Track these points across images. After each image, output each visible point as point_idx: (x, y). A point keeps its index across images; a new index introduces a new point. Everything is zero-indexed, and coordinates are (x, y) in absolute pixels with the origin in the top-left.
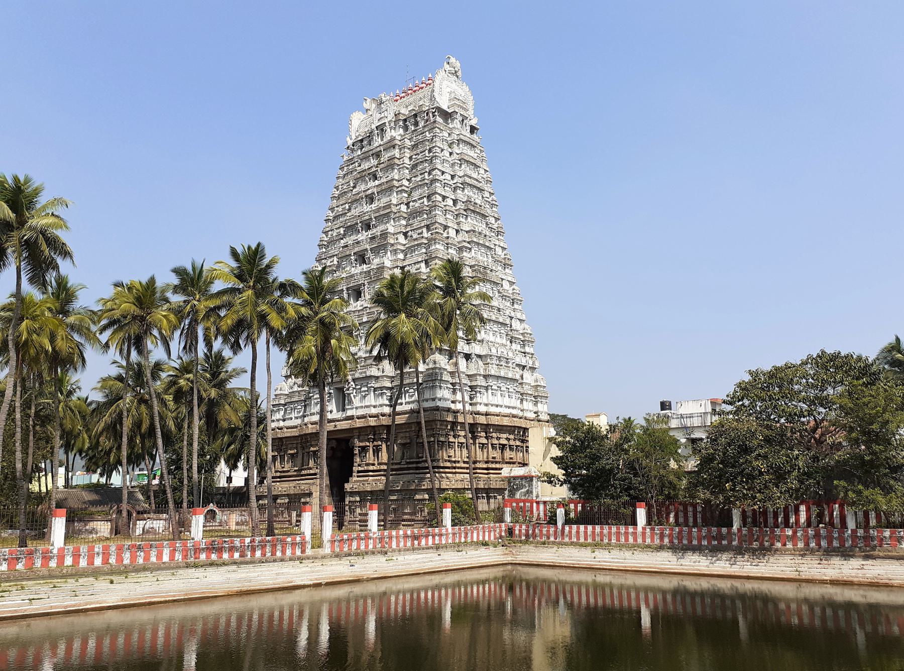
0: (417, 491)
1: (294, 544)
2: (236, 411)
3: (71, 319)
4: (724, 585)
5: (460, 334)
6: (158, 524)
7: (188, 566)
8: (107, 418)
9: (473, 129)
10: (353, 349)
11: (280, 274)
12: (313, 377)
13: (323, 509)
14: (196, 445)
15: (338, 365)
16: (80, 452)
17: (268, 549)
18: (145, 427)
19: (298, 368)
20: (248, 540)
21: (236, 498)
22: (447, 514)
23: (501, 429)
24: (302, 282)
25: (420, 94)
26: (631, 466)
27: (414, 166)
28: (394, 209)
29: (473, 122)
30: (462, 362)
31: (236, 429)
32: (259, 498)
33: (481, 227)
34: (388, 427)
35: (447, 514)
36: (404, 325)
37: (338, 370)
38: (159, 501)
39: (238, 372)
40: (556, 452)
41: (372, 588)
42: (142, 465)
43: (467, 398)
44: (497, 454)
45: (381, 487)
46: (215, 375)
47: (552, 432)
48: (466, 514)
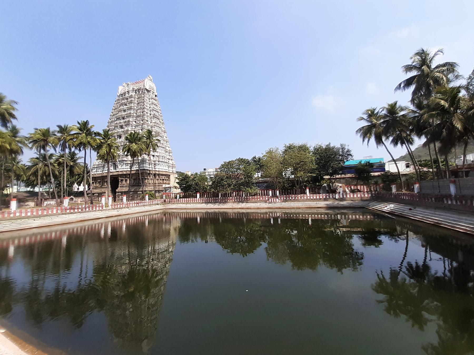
0: (138, 191)
1: (99, 207)
2: (80, 169)
3: (17, 139)
4: (217, 211)
5: (151, 149)
6: (53, 202)
7: (63, 214)
8: (32, 170)
9: (156, 96)
10: (118, 153)
11: (94, 130)
12: (106, 160)
13: (109, 196)
14: (65, 179)
15: (114, 157)
16: (23, 181)
17: (91, 208)
18: (47, 173)
19: (101, 157)
20: (84, 206)
21: (81, 194)
22: (147, 197)
23: (163, 175)
24: (102, 132)
25: (140, 84)
26: (196, 184)
27: (138, 103)
28: (132, 114)
29: (156, 94)
30: (152, 157)
31: (80, 174)
32: (87, 194)
33: (158, 122)
34: (129, 174)
35: (147, 197)
36: (134, 146)
37: (114, 158)
38: (52, 196)
39: (80, 158)
40: (177, 181)
41: (124, 217)
42: (47, 185)
43: (153, 167)
44: (162, 181)
45: (127, 190)
46: (72, 158)
47: (177, 176)
48: (152, 197)
